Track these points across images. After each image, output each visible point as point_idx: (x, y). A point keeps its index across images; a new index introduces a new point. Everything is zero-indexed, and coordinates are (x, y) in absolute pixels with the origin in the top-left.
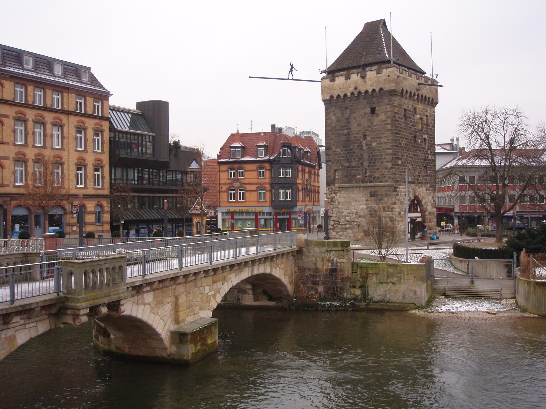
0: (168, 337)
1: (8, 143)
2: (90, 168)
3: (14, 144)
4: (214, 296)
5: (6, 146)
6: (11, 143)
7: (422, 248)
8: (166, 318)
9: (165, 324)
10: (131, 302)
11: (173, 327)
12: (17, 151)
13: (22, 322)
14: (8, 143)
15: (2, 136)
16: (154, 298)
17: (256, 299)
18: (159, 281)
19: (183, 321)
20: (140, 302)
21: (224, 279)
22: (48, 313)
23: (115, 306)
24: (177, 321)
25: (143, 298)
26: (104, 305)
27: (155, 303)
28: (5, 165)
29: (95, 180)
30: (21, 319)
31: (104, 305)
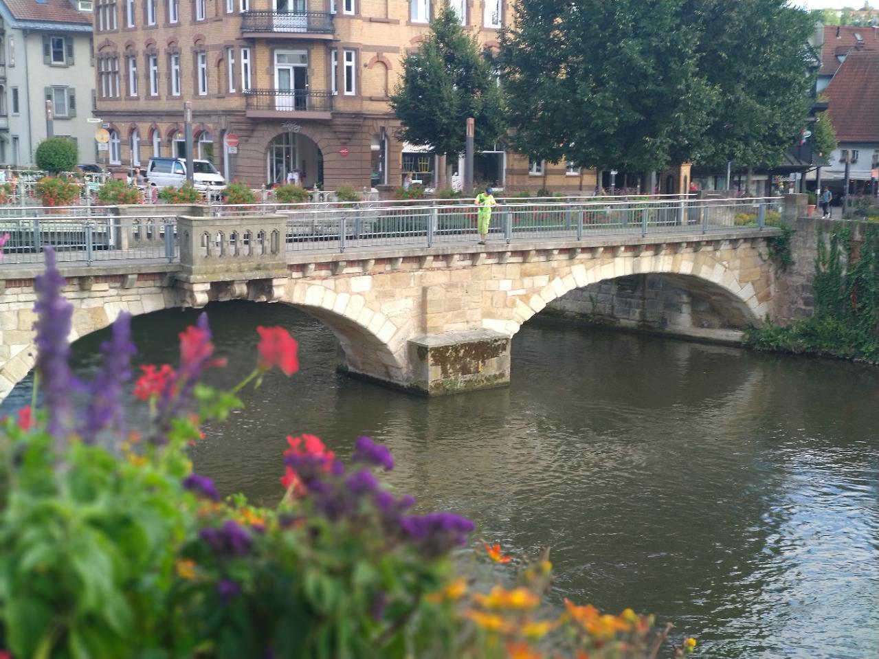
0: (402, 350)
1: (397, 22)
2: (187, 55)
3: (409, 23)
4: (526, 298)
5: (394, 28)
6: (403, 22)
7: (176, 205)
8: (399, 320)
9: (398, 330)
10: (322, 288)
11: (413, 336)
12: (414, 35)
13: (113, 292)
14: (397, 22)
15: (387, 8)
16: (373, 286)
17: (698, 323)
18: (404, 258)
19: (435, 329)
20: (341, 288)
21: (553, 274)
22: (158, 284)
23: (264, 285)
24: (424, 328)
25: (348, 284)
26: (241, 281)
27: (374, 293)
28: (392, 62)
29: (357, 77)
30: (111, 288)
31: (241, 281)
